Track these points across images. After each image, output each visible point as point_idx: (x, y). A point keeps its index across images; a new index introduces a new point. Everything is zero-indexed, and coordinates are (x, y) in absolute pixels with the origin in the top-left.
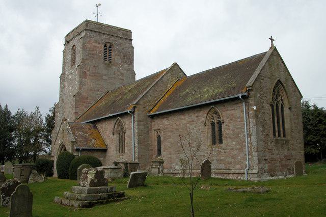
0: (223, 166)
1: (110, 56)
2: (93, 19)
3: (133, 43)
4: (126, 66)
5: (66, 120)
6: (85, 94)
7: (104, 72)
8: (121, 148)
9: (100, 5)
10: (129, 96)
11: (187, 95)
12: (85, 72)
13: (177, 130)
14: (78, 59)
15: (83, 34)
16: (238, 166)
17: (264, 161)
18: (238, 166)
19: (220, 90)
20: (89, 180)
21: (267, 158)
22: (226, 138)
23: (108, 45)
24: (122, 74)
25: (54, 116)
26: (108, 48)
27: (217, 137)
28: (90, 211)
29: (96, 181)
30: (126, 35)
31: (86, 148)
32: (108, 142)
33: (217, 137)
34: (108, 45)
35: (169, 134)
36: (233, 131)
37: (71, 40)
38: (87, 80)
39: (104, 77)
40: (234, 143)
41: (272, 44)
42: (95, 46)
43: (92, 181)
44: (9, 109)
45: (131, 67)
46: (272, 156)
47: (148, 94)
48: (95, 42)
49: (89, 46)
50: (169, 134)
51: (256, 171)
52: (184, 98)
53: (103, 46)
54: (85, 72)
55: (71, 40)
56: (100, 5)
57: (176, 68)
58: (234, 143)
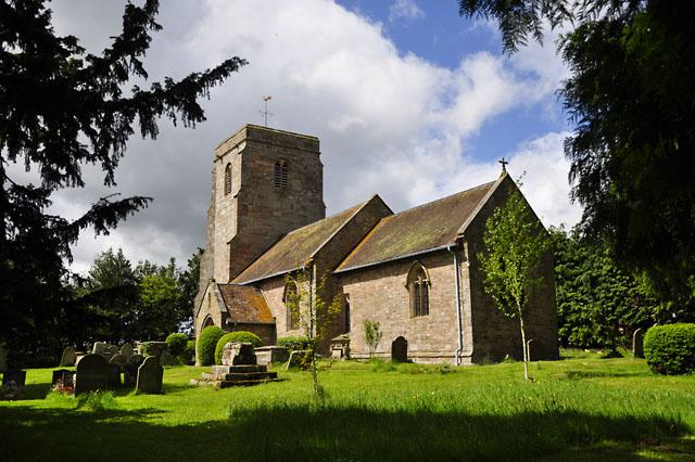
0: (428, 347)
1: (285, 180)
2: (260, 122)
3: (322, 158)
4: (310, 194)
5: (214, 281)
6: (245, 241)
7: (276, 205)
8: (293, 322)
9: (269, 98)
10: (306, 246)
11: (386, 245)
12: (246, 206)
13: (371, 295)
14: (236, 186)
15: (242, 147)
16: (448, 347)
17: (484, 340)
18: (448, 347)
19: (427, 238)
20: (232, 357)
21: (488, 335)
22: (433, 306)
23: (282, 163)
24: (304, 208)
25: (197, 273)
26: (282, 169)
27: (421, 306)
28: (226, 391)
29: (242, 357)
30: (311, 146)
31: (243, 321)
32: (276, 313)
33: (421, 306)
34: (282, 163)
35: (361, 301)
36: (442, 296)
37: (225, 154)
38: (250, 218)
39: (275, 214)
40: (443, 314)
41: (504, 169)
42: (261, 165)
43: (236, 357)
44: (127, 256)
45: (318, 196)
46: (500, 333)
47: (622, 379)
48: (262, 158)
49: (252, 165)
50: (361, 301)
51: (470, 354)
52: (381, 249)
53: (273, 165)
54: (246, 206)
55: (225, 154)
56: (269, 98)
57: (377, 203)
58: (443, 314)
